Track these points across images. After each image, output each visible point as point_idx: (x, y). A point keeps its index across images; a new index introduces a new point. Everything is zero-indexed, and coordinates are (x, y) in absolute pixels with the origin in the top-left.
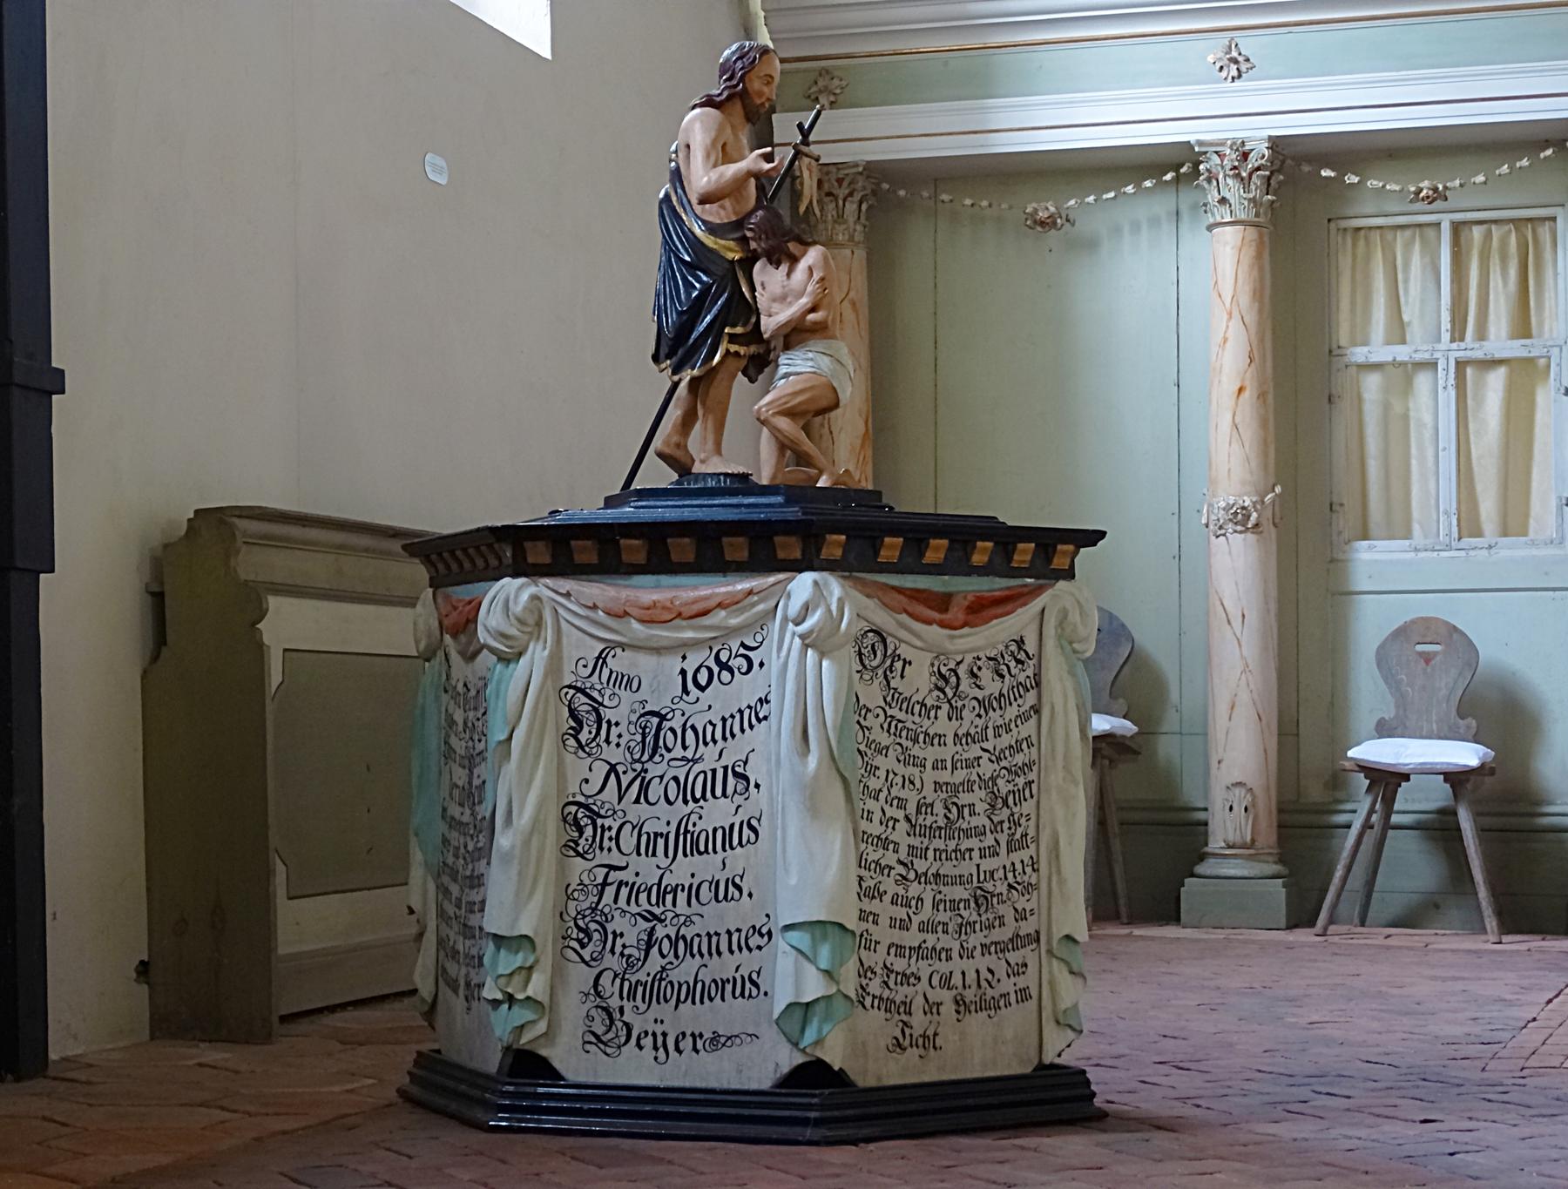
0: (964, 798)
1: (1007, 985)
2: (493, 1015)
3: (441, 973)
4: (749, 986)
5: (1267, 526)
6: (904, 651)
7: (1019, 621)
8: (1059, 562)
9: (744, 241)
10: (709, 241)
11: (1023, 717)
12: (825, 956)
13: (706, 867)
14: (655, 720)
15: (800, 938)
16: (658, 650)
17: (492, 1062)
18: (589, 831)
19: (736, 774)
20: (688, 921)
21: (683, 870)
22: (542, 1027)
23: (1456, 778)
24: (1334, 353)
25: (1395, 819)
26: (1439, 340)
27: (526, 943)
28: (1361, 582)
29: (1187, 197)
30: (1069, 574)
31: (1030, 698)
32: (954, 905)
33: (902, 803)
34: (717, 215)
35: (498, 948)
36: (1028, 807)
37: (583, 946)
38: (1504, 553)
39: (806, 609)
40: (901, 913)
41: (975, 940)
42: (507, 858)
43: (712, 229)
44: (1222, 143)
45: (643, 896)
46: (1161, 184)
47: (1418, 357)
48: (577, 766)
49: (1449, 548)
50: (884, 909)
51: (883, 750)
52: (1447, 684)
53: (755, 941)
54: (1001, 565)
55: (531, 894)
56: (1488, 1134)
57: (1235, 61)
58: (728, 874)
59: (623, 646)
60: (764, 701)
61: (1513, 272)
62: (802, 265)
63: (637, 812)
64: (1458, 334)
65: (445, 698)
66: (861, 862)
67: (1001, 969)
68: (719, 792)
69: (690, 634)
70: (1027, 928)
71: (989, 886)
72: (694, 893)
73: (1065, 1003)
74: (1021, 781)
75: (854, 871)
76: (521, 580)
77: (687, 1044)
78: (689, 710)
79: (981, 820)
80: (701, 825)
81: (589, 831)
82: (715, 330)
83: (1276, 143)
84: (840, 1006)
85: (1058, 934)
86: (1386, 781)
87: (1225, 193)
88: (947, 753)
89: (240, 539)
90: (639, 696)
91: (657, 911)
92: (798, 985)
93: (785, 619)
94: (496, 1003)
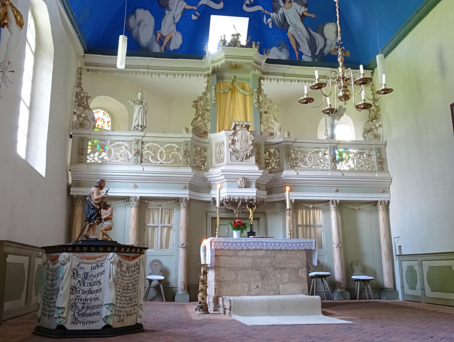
0: (129, 285)
1: (133, 312)
2: (56, 320)
3: (43, 313)
4: (98, 313)
6: (123, 264)
7: (137, 260)
8: (142, 252)
9: (100, 206)
10: (95, 205)
11: (137, 273)
13: (93, 296)
14: (86, 274)
15: (107, 306)
16: (88, 264)
17: (54, 327)
18: (74, 291)
19: (99, 282)
20: (90, 304)
21: (89, 297)
22: (64, 321)
23: (160, 281)
24: (145, 224)
25: (151, 286)
26: (159, 223)
27: (63, 309)
29: (127, 203)
30: (143, 253)
31: (138, 271)
32: (127, 300)
33: (121, 286)
34: (96, 202)
35: (58, 310)
36: (137, 286)
37: (72, 308)
39: (111, 258)
40: (120, 302)
41: (129, 305)
42: (61, 295)
43: (95, 204)
44: (133, 196)
45: (83, 301)
46: (124, 201)
47: (156, 225)
48: (73, 281)
50: (118, 301)
51: (119, 278)
52: (159, 268)
53: (100, 307)
54: (135, 252)
55: (65, 300)
58: (96, 297)
59: (82, 263)
61: (168, 215)
62: (109, 210)
63: (82, 288)
64: (161, 223)
65: (47, 271)
66: (116, 295)
67: (132, 310)
68: (96, 284)
69: (93, 261)
70: (136, 303)
71: (132, 297)
72: (91, 300)
73: (140, 314)
74: (136, 282)
75: (115, 296)
76: (67, 253)
77: (88, 323)
78: (92, 272)
79: (131, 288)
80: (93, 290)
81: (74, 291)
82: (95, 218)
83: (140, 197)
84: (112, 316)
85: (140, 304)
86: (151, 281)
88: (127, 278)
89: (5, 245)
90: (84, 270)
91: (85, 303)
92: (107, 313)
93: (108, 259)
94: (56, 318)
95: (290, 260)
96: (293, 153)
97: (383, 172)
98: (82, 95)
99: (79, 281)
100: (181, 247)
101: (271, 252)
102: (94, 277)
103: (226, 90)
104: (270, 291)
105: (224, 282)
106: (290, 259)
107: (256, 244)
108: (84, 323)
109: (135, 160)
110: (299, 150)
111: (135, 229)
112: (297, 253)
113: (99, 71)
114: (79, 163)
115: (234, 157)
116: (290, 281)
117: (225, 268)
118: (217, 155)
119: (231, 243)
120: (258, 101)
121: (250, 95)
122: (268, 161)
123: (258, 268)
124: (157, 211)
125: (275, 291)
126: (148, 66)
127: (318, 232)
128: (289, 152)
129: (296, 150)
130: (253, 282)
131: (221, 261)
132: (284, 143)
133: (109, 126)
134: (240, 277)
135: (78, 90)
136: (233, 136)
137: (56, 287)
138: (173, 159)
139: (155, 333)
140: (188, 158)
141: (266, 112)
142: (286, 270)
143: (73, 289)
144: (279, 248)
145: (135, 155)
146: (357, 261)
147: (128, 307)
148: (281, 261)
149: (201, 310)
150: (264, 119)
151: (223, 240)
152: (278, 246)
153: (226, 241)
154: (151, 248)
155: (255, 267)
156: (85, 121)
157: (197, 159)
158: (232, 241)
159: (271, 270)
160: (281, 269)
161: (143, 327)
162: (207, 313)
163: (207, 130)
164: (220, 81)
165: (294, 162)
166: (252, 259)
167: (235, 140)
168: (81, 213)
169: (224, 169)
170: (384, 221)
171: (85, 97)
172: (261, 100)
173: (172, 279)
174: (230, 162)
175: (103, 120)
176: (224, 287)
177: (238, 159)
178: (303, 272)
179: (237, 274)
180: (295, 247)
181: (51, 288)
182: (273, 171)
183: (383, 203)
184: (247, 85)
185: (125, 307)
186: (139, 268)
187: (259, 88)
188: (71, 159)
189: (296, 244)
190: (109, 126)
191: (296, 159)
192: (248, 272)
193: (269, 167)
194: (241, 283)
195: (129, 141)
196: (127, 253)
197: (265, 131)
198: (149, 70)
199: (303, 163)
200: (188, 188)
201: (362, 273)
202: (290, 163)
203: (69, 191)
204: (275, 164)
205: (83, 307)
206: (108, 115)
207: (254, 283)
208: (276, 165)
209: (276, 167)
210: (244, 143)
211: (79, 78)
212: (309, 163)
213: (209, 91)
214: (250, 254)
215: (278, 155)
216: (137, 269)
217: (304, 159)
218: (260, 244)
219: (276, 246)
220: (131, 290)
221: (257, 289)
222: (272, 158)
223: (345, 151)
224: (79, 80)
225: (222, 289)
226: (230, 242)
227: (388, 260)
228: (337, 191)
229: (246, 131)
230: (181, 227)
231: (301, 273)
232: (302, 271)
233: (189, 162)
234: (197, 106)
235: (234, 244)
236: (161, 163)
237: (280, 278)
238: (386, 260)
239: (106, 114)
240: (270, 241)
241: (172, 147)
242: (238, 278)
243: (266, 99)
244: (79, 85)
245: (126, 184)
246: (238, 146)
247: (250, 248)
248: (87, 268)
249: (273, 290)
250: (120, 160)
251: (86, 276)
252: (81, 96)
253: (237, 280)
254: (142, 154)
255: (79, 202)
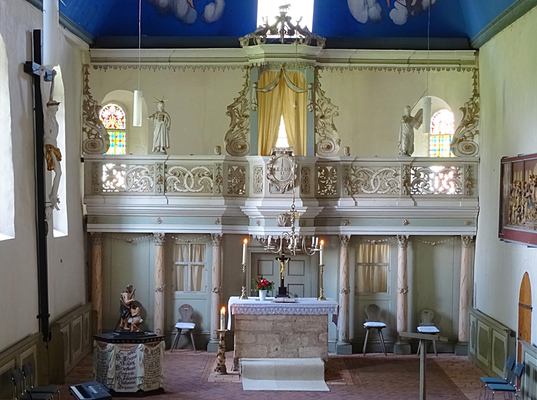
1: (157, 380)
4: (134, 382)
5: (164, 291)
6: (149, 350)
7: (158, 346)
9: (130, 306)
12: (142, 380)
13: (130, 371)
16: (125, 351)
20: (128, 376)
21: (128, 372)
22: (113, 387)
24: (173, 263)
25: (182, 333)
26: (188, 261)
28: (176, 297)
31: (159, 353)
32: (152, 373)
33: (148, 364)
36: (159, 363)
38: (197, 294)
41: (154, 377)
44: (158, 233)
47: (185, 264)
48: (117, 362)
49: (189, 293)
50: (147, 375)
52: (189, 314)
54: (157, 341)
56: (202, 393)
57: (160, 221)
60: (136, 356)
61: (199, 251)
64: (191, 261)
70: (158, 375)
72: (129, 374)
79: (155, 365)
86: (180, 330)
87: (158, 241)
92: (139, 382)
94: (108, 385)
95: (311, 324)
96: (353, 175)
97: (471, 198)
98: (91, 104)
99: (121, 362)
100: (213, 292)
101: (292, 316)
102: (130, 359)
103: (271, 86)
104: (289, 353)
105: (244, 345)
106: (311, 323)
107: (276, 309)
108: (125, 388)
109: (158, 189)
110: (361, 171)
111: (161, 271)
112: (319, 317)
113: (108, 67)
114: (94, 195)
115: (273, 188)
116: (310, 344)
117: (245, 331)
118: (255, 182)
119: (251, 309)
120: (312, 102)
121: (304, 92)
122: (324, 182)
123: (278, 332)
124: (185, 247)
125: (294, 354)
126: (170, 58)
127: (384, 274)
128: (348, 174)
129: (358, 171)
130: (273, 345)
131: (242, 325)
132: (341, 163)
133: (123, 123)
134: (259, 340)
135: (86, 98)
136: (272, 165)
137: (105, 365)
138: (203, 187)
139: (172, 395)
140: (220, 186)
141: (322, 117)
142: (307, 334)
143: (117, 367)
144: (300, 313)
145: (158, 183)
146: (427, 309)
147: (153, 378)
148: (301, 325)
149: (220, 371)
150: (320, 126)
151: (243, 306)
152: (299, 311)
153: (246, 306)
154: (180, 290)
155: (275, 331)
156: (97, 140)
157: (233, 181)
158: (252, 306)
159: (291, 334)
160: (302, 333)
161: (164, 390)
162: (225, 374)
163: (245, 143)
164: (264, 72)
165: (354, 187)
166: (272, 323)
167: (275, 169)
168: (100, 252)
169: (261, 206)
170: (466, 260)
171: (95, 107)
172: (317, 99)
173: (204, 325)
174: (269, 194)
175: (116, 116)
176: (244, 349)
177: (278, 190)
178: (324, 336)
179: (256, 337)
180: (316, 312)
181: (102, 365)
182: (328, 197)
183: (467, 238)
184: (301, 75)
185: (151, 378)
186: (160, 351)
187: (315, 81)
188: (85, 189)
189: (317, 309)
190: (123, 123)
191: (358, 182)
192: (268, 335)
193: (324, 189)
194: (261, 346)
195: (150, 165)
196: (151, 342)
197: (321, 142)
198: (171, 63)
199: (366, 187)
200: (221, 223)
201: (432, 323)
202: (348, 189)
203: (85, 228)
204: (332, 187)
205: (124, 379)
206: (121, 109)
207: (273, 346)
208: (333, 187)
209: (332, 190)
210: (285, 172)
211: (85, 79)
212: (373, 188)
213: (249, 90)
214: (270, 318)
215: (336, 175)
216: (158, 352)
217: (367, 182)
218: (280, 309)
219: (297, 311)
220: (154, 366)
221: (277, 351)
222: (329, 178)
223: (424, 169)
224: (85, 83)
225: (242, 351)
226: (250, 308)
227: (464, 308)
228: (407, 223)
229: (287, 157)
230: (213, 268)
231: (321, 337)
232: (323, 335)
233: (222, 191)
234: (233, 112)
235: (254, 310)
236: (189, 191)
237: (300, 341)
238: (463, 309)
239: (120, 107)
240: (291, 306)
241: (201, 171)
242: (258, 341)
243: (324, 98)
244: (86, 91)
245: (148, 218)
246: (278, 176)
247: (269, 313)
248: (126, 354)
249: (292, 352)
250: (140, 188)
251: (125, 358)
252: (89, 106)
253: (257, 343)
254: (165, 181)
255: (97, 240)
